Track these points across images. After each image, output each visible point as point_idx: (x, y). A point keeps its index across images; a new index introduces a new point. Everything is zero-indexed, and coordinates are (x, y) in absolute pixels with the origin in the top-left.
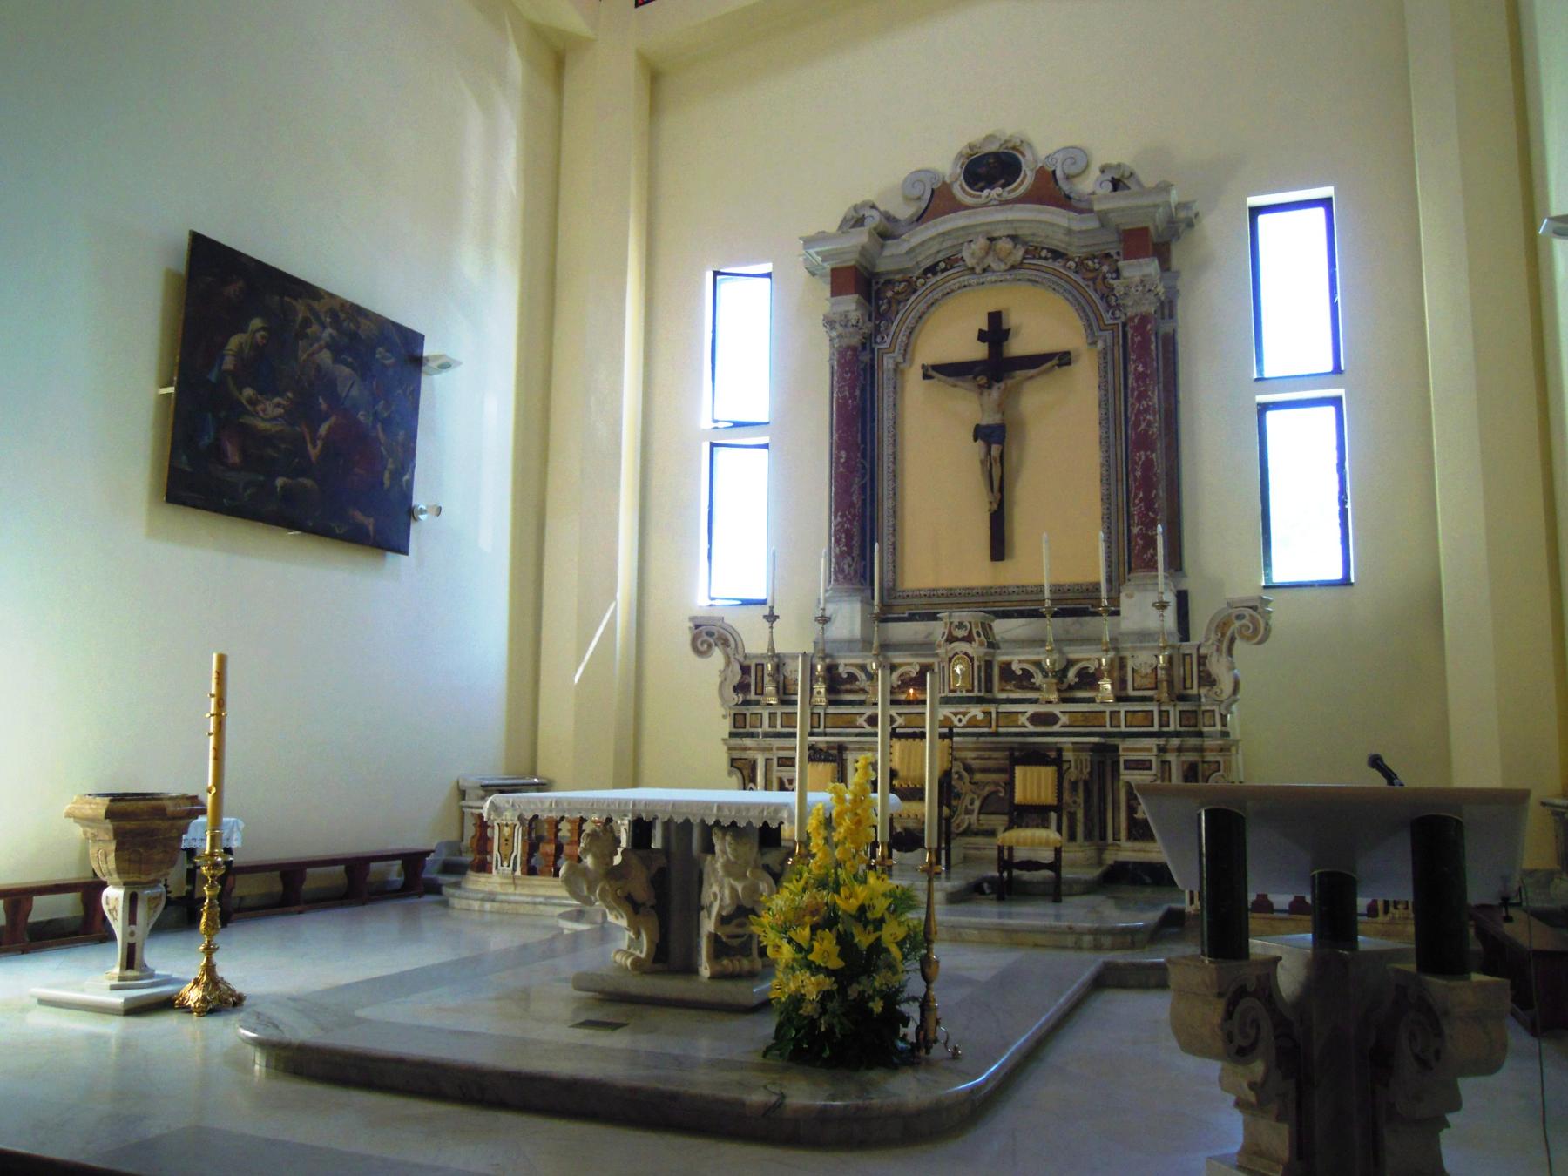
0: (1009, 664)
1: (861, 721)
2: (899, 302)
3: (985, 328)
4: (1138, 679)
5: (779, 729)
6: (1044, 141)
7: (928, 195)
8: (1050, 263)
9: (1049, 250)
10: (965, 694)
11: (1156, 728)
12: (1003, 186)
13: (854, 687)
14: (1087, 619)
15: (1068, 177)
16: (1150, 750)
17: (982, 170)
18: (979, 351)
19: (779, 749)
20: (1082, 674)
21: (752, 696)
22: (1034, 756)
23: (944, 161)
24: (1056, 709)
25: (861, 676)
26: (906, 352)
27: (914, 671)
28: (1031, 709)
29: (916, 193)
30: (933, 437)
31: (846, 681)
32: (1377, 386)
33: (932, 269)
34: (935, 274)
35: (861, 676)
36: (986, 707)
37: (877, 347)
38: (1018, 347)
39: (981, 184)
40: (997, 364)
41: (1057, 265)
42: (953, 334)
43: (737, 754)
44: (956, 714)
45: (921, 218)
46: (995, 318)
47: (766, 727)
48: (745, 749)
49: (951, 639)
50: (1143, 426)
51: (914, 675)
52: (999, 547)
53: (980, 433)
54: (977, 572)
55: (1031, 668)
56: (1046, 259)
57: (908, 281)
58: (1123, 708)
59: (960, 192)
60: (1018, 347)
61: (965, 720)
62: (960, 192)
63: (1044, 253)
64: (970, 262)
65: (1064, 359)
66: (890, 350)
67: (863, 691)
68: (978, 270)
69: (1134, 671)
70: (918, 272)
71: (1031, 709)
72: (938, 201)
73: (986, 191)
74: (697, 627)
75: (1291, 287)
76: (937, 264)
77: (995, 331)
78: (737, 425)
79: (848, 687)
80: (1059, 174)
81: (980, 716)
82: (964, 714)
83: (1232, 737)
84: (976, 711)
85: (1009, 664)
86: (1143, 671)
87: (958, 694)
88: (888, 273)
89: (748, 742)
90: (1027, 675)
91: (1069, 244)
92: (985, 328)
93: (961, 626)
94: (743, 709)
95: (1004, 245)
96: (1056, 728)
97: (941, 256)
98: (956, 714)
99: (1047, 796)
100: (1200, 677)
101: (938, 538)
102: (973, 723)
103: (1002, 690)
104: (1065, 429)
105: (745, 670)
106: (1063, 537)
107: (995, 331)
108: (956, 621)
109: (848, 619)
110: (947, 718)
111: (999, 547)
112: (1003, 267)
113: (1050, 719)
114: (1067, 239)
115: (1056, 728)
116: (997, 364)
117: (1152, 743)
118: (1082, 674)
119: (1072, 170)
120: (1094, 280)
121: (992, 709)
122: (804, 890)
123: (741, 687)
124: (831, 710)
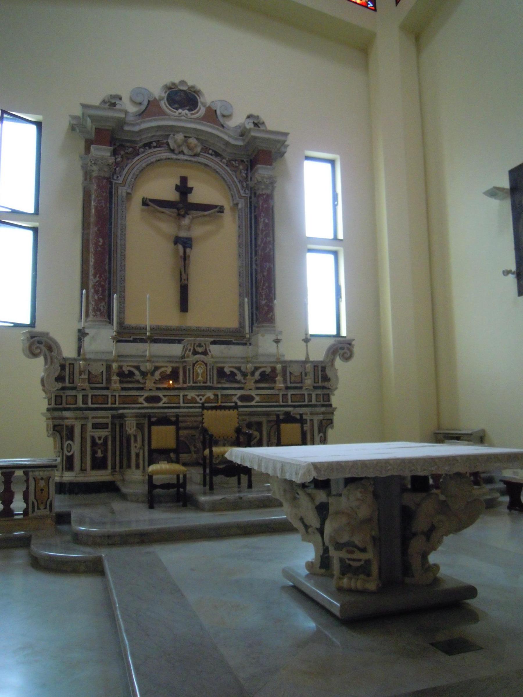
0: (223, 368)
1: (141, 400)
2: (128, 159)
3: (179, 184)
4: (293, 378)
5: (90, 405)
6: (210, 96)
7: (146, 103)
8: (213, 157)
9: (213, 151)
10: (202, 384)
11: (109, 405)
12: (190, 110)
13: (133, 380)
14: (232, 346)
15: (224, 116)
16: (108, 417)
17: (177, 98)
18: (172, 195)
19: (93, 418)
20: (263, 374)
21: (67, 384)
22: (164, 421)
23: (157, 90)
24: (253, 393)
25: (137, 373)
26: (133, 187)
27: (169, 370)
28: (239, 393)
29: (139, 100)
30: (145, 243)
31: (126, 376)
32: (359, 250)
33: (148, 145)
34: (150, 148)
35: (137, 373)
36: (216, 392)
37: (114, 182)
38: (193, 198)
39: (176, 106)
40: (182, 205)
41: (217, 159)
42: (162, 186)
43: (57, 422)
44: (198, 396)
45: (142, 114)
46: (184, 180)
47: (80, 404)
48: (63, 418)
49: (195, 353)
50: (268, 250)
51: (168, 373)
52: (184, 305)
53: (177, 240)
54: (171, 318)
55: (235, 371)
56: (211, 155)
57: (134, 148)
58: (290, 392)
59: (164, 105)
60: (193, 198)
61: (203, 399)
62: (164, 105)
63: (210, 152)
64: (172, 145)
65: (221, 210)
66: (124, 184)
67: (138, 382)
68: (176, 152)
69: (290, 373)
70: (141, 144)
71: (239, 393)
72: (151, 108)
73: (180, 111)
74: (32, 337)
75: (317, 195)
76: (151, 143)
77: (184, 189)
78: (14, 212)
79: (129, 379)
80: (218, 112)
81: (212, 397)
82: (203, 396)
83: (333, 406)
84: (210, 394)
85: (223, 368)
86: (296, 374)
87: (198, 384)
88: (123, 140)
89: (66, 414)
90: (233, 374)
91: (224, 150)
92: (179, 184)
93: (200, 345)
94: (61, 393)
95: (193, 141)
96: (253, 403)
97: (154, 139)
98: (198, 396)
99: (171, 443)
100: (322, 377)
101: (148, 299)
102: (208, 400)
103: (219, 383)
104: (219, 248)
105: (63, 367)
106: (217, 302)
107: (184, 189)
108: (197, 343)
109: (102, 341)
110: (193, 398)
111: (184, 305)
112: (191, 153)
113: (250, 398)
114: (223, 147)
115: (253, 403)
116: (182, 205)
117: (109, 413)
118: (263, 374)
119: (226, 113)
120: (235, 171)
121: (219, 393)
122: (348, 498)
123: (60, 379)
124: (124, 393)
